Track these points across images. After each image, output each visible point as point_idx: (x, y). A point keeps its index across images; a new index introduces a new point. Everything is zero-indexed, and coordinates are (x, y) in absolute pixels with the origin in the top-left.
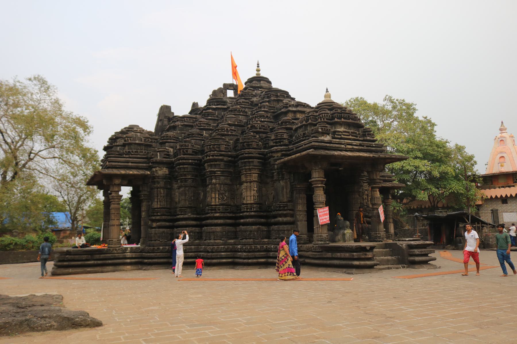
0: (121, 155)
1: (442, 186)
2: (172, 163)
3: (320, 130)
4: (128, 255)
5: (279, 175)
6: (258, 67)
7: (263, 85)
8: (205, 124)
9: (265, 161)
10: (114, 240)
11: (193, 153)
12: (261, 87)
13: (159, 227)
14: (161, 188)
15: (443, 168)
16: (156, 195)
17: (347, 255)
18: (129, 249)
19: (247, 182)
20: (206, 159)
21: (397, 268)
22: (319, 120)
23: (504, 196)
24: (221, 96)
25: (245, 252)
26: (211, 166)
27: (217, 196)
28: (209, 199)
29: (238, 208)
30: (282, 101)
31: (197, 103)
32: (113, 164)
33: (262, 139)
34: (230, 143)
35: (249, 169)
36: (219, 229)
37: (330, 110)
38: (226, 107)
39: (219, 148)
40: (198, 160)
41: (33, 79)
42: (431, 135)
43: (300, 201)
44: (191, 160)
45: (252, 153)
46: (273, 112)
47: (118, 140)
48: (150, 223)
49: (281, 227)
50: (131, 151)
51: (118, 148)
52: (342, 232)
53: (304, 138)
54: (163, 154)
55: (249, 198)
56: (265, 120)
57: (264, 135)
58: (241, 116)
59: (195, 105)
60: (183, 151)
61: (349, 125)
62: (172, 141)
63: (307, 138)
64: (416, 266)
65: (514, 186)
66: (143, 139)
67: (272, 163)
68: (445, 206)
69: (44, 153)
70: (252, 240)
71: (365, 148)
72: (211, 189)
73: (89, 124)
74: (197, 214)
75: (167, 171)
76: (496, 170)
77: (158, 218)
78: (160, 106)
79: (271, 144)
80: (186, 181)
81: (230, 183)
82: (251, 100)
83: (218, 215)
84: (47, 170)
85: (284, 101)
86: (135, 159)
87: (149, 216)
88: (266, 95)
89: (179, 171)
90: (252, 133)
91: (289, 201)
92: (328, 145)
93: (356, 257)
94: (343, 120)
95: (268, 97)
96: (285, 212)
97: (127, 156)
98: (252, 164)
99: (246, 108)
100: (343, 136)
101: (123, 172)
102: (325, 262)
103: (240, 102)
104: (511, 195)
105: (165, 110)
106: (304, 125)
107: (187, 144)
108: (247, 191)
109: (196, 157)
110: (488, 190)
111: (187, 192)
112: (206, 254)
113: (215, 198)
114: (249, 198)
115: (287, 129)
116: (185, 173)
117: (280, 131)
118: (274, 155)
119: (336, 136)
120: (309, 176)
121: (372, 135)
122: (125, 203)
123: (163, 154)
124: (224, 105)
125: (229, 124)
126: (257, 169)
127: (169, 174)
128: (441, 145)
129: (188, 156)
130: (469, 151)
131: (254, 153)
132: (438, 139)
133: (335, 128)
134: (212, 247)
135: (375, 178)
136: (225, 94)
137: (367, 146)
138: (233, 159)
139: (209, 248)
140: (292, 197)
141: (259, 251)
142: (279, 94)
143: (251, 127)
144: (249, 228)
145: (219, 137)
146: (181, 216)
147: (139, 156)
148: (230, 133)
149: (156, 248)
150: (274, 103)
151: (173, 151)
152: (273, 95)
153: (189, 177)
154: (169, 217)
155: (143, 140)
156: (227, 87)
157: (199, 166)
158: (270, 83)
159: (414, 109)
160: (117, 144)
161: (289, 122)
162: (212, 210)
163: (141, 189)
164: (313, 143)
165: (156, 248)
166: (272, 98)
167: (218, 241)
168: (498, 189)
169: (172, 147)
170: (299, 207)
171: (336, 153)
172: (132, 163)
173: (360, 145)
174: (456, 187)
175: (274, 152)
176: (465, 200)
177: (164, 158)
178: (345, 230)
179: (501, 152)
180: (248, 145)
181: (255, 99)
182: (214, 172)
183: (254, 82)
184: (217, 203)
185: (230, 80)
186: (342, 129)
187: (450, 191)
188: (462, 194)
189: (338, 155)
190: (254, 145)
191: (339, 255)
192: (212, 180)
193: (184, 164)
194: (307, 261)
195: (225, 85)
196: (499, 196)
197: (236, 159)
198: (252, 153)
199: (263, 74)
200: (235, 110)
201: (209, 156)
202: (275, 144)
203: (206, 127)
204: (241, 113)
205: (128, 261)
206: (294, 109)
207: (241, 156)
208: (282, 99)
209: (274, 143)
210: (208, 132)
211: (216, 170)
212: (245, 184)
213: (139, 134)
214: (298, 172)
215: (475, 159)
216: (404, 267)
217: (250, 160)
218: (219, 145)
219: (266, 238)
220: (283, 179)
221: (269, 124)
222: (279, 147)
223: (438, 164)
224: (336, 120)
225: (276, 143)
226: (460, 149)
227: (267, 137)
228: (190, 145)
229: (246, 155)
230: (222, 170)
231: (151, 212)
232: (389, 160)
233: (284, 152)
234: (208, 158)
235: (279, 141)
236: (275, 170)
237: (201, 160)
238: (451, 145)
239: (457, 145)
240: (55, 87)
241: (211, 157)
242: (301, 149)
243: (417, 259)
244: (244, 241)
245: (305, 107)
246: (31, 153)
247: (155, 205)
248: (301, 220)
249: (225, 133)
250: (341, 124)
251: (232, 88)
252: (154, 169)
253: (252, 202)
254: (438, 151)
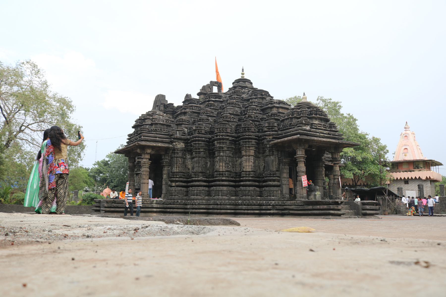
0: (150, 132)
1: (363, 168)
2: (188, 139)
3: (304, 122)
4: (155, 205)
6: (243, 71)
9: (260, 141)
10: (145, 194)
12: (246, 87)
13: (177, 186)
14: (179, 157)
15: (364, 155)
16: (176, 162)
17: (325, 207)
18: (155, 201)
19: (246, 156)
20: (215, 138)
21: (355, 218)
22: (302, 115)
23: (406, 178)
25: (245, 205)
26: (220, 143)
27: (224, 165)
28: (218, 167)
29: (239, 175)
30: (265, 98)
31: (190, 95)
32: (146, 138)
33: (256, 126)
35: (249, 146)
36: (225, 188)
37: (308, 108)
38: (221, 100)
39: (226, 130)
41: (25, 63)
42: (356, 129)
43: (285, 171)
46: (261, 107)
47: (146, 121)
48: (169, 183)
49: (272, 188)
51: (147, 126)
52: (313, 193)
54: (181, 132)
55: (248, 167)
57: (258, 123)
59: (187, 96)
61: (321, 119)
62: (186, 123)
63: (293, 127)
64: (367, 217)
65: (414, 171)
66: (165, 121)
67: (266, 143)
68: (365, 184)
69: (34, 126)
70: (249, 197)
71: (332, 136)
72: (220, 159)
73: (72, 104)
74: (206, 178)
76: (401, 158)
77: (177, 179)
80: (199, 153)
81: (232, 156)
83: (224, 178)
84: (33, 139)
87: (169, 177)
89: (195, 145)
90: (251, 121)
91: (277, 171)
92: (309, 132)
93: (332, 208)
94: (318, 116)
95: (255, 95)
96: (274, 178)
98: (250, 143)
100: (318, 127)
101: (154, 144)
102: (307, 212)
104: (412, 178)
108: (246, 162)
110: (394, 173)
111: (200, 161)
112: (216, 206)
113: (223, 166)
114: (248, 167)
115: (276, 119)
118: (267, 137)
119: (313, 127)
120: (295, 153)
121: (335, 127)
122: (91, 172)
123: (181, 132)
124: (220, 99)
125: (230, 113)
128: (363, 137)
130: (383, 142)
131: (253, 135)
132: (359, 132)
133: (312, 121)
134: (220, 201)
135: (337, 157)
136: (212, 89)
137: (333, 135)
139: (218, 202)
140: (279, 168)
141: (255, 205)
142: (263, 94)
143: (248, 116)
144: (248, 188)
145: (226, 122)
146: (196, 179)
147: (163, 133)
149: (176, 201)
154: (185, 179)
156: (213, 84)
157: (210, 143)
158: (251, 83)
159: (340, 107)
160: (147, 123)
161: (277, 115)
162: (219, 175)
163: (163, 157)
164: (300, 131)
165: (176, 201)
167: (224, 197)
168: (402, 173)
169: (186, 128)
170: (284, 175)
171: (316, 138)
173: (328, 134)
174: (373, 169)
175: (266, 135)
176: (379, 180)
177: (182, 135)
178: (316, 192)
179: (405, 145)
180: (248, 130)
181: (244, 96)
183: (241, 83)
184: (224, 170)
185: (215, 80)
186: (317, 122)
187: (369, 172)
188: (377, 175)
189: (317, 140)
191: (318, 207)
193: (199, 141)
194: (291, 212)
195: (211, 82)
196: (403, 178)
197: (237, 139)
199: (246, 77)
205: (155, 210)
207: (241, 137)
209: (267, 129)
212: (245, 157)
213: (161, 117)
214: (287, 152)
215: (387, 148)
216: (359, 217)
219: (259, 196)
220: (273, 155)
221: (260, 115)
223: (360, 151)
224: (314, 115)
225: (269, 129)
226: (376, 141)
227: (261, 124)
231: (171, 175)
232: (345, 145)
234: (218, 137)
235: (271, 128)
236: (267, 148)
237: (210, 139)
238: (369, 137)
239: (374, 137)
240: (44, 71)
241: (221, 137)
243: (368, 212)
244: (244, 197)
246: (22, 125)
247: (175, 170)
248: (286, 184)
250: (316, 119)
251: (217, 85)
252: (174, 143)
253: (250, 170)
254: (361, 142)
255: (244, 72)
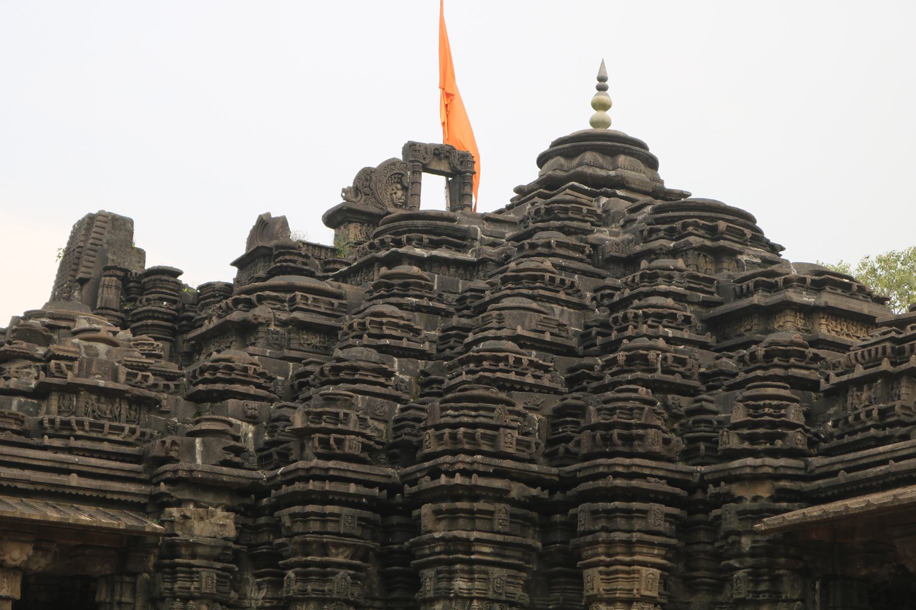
2: (258, 489)
5: (757, 582)
6: (602, 88)
7: (629, 174)
8: (397, 326)
9: (694, 508)
11: (365, 455)
12: (621, 183)
20: (426, 483)
24: (390, 199)
26: (452, 516)
30: (733, 254)
31: (283, 222)
33: (675, 417)
34: (531, 422)
35: (629, 544)
38: (469, 256)
39: (493, 439)
40: (382, 487)
44: (357, 482)
45: (643, 476)
46: (706, 304)
50: (73, 418)
51: (15, 401)
53: (888, 431)
54: (218, 445)
56: (679, 334)
57: (685, 402)
58: (557, 308)
60: (324, 443)
62: (252, 390)
66: (123, 372)
67: (732, 523)
75: (230, 523)
78: (81, 215)
79: (733, 442)
80: (324, 577)
82: (591, 238)
85: (743, 258)
86: (93, 461)
88: (658, 221)
89: (298, 528)
90: (643, 391)
95: (671, 234)
97: (57, 443)
98: (638, 524)
99: (575, 271)
103: (548, 245)
105: (107, 236)
106: (884, 374)
107: (341, 411)
109: (377, 470)
116: (326, 539)
117: (771, 391)
118: (737, 490)
123: (218, 445)
124: (461, 248)
125: (516, 339)
126: (661, 545)
127: (236, 542)
129: (344, 465)
131: (654, 475)
136: (412, 190)
138: (545, 494)
142: (722, 225)
143: (630, 360)
145: (494, 392)
147: (106, 446)
148: (529, 379)
150: (701, 260)
151: (257, 434)
152: (696, 225)
153: (340, 559)
155: (122, 377)
156: (419, 158)
157: (391, 513)
158: (652, 163)
161: (802, 356)
166: (695, 240)
169: (252, 419)
172: (81, 474)
177: (225, 463)
180: (628, 440)
181: (604, 235)
182: (467, 545)
190: (653, 440)
192: (450, 579)
193: (324, 498)
195: (411, 148)
197: (558, 496)
198: (643, 476)
199: (621, 122)
200: (535, 279)
201: (451, 475)
202: (746, 445)
203: (405, 343)
204: (562, 296)
206: (808, 299)
208: (737, 247)
209: (743, 438)
210: (410, 363)
211: (475, 535)
213: (102, 347)
217: (636, 505)
218: (496, 428)
222: (769, 461)
228: (353, 416)
229: (619, 482)
230: (499, 538)
233: (783, 483)
234: (443, 480)
235: (765, 433)
236: (740, 555)
237: (393, 488)
241: (458, 479)
242: (877, 477)
245: (853, 296)
249: (512, 376)
251: (444, 167)
252: (175, 512)
255: (613, 94)
